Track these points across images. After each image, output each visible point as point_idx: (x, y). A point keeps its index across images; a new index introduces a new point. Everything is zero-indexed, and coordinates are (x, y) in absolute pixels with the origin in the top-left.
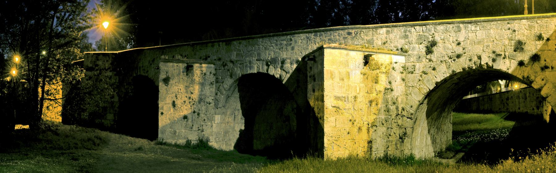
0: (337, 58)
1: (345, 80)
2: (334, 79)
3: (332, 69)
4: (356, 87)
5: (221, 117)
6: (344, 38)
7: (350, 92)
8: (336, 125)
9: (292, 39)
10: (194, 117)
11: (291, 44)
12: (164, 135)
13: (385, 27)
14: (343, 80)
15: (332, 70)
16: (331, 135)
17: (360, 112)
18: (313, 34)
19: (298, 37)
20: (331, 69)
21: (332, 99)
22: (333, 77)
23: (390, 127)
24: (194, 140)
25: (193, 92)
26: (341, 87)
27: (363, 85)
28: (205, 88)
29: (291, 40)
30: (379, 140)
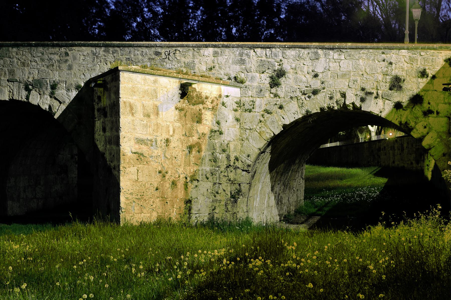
0: (140, 86)
1: (152, 117)
2: (135, 115)
3: (132, 101)
4: (168, 127)
6: (149, 59)
7: (159, 134)
8: (138, 179)
9: (69, 53)
11: (66, 61)
13: (212, 47)
14: (149, 116)
18: (103, 49)
20: (130, 100)
21: (132, 142)
23: (218, 181)
26: (146, 126)
29: (67, 54)
30: (201, 199)
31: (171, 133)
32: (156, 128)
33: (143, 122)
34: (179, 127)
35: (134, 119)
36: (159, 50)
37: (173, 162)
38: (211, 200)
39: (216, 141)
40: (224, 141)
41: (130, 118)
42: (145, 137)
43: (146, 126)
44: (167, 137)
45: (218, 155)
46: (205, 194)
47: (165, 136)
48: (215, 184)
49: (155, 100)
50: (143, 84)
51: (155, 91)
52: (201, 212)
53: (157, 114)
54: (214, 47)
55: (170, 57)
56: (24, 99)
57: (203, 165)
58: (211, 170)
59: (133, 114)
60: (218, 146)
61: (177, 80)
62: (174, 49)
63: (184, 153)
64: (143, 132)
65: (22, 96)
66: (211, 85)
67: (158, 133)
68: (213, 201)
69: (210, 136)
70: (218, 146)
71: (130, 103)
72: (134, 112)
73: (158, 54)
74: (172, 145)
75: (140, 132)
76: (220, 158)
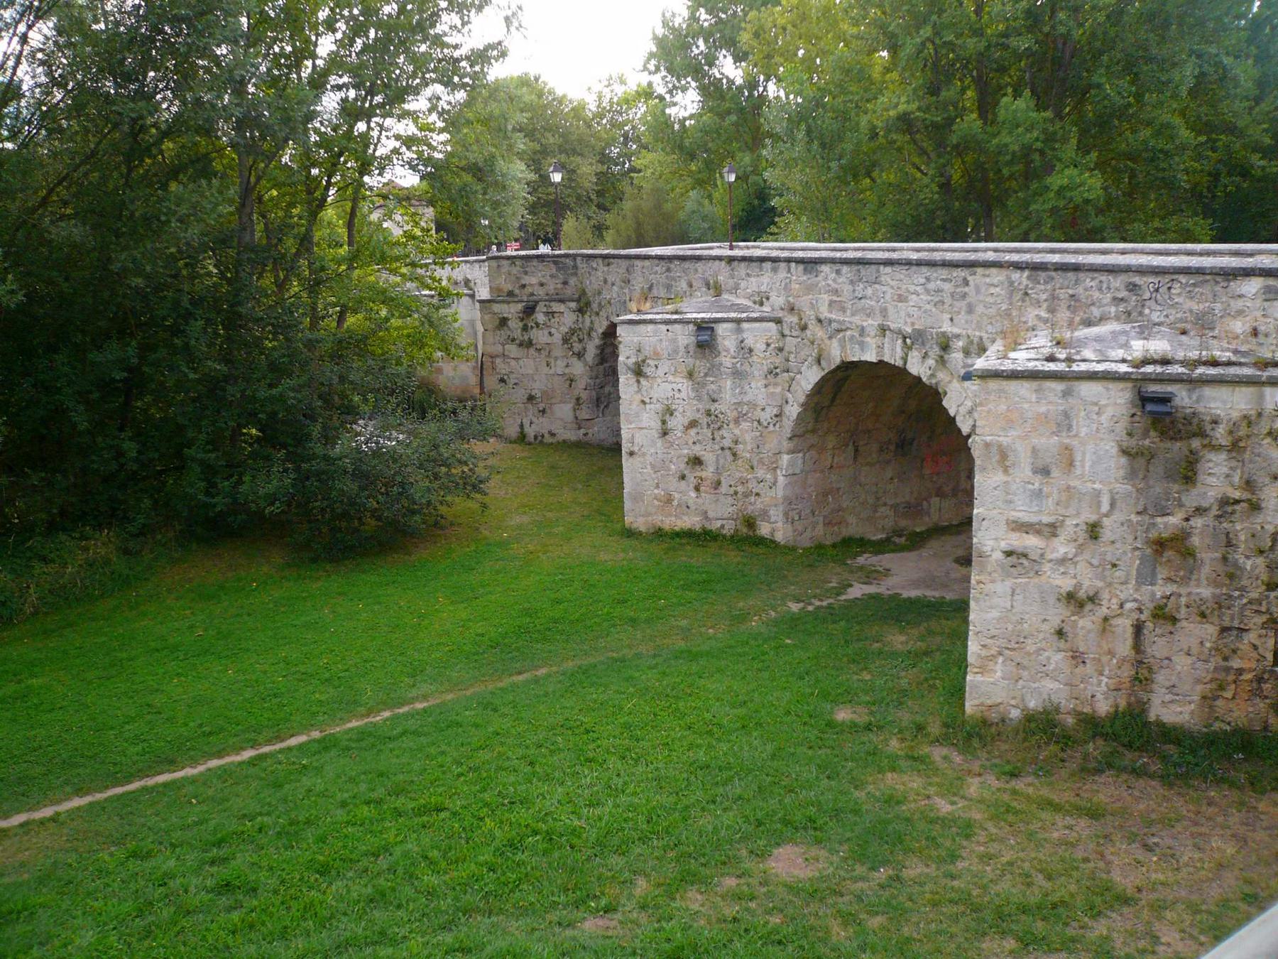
0: (1026, 406)
1: (1055, 473)
2: (1011, 471)
3: (1004, 441)
4: (1098, 494)
5: (804, 458)
6: (1115, 299)
7: (1071, 511)
8: (1012, 606)
9: (969, 278)
10: (722, 461)
11: (964, 296)
12: (637, 515)
13: (1260, 275)
14: (1045, 472)
15: (1005, 444)
16: (993, 632)
17: (1107, 573)
18: (1026, 273)
19: (984, 275)
20: (1001, 439)
21: (1001, 530)
22: (1007, 464)
23: (1236, 624)
24: (725, 516)
25: (715, 396)
26: (1038, 494)
27: (1130, 487)
28: (753, 385)
29: (966, 283)
30: (1182, 663)
31: (1105, 507)
32: (1063, 499)
33: (1030, 486)
34: (1129, 495)
35: (1009, 479)
36: (1137, 279)
37: (1107, 573)
38: (1211, 666)
39: (1238, 528)
40: (1262, 527)
41: (998, 477)
42: (1033, 519)
43: (1038, 494)
44: (1093, 518)
45: (1242, 560)
46: (1195, 651)
47: (1090, 516)
48: (1224, 630)
49: (1064, 434)
50: (1034, 400)
51: (1066, 415)
52: (1179, 692)
53: (1071, 464)
54: (1265, 276)
55: (1159, 296)
56: (899, 363)
57: (1193, 583)
58: (1214, 595)
59: (1006, 471)
60: (1243, 538)
61: (1130, 385)
62: (1168, 278)
63: (1137, 553)
64: (1030, 507)
65: (893, 354)
66: (1231, 389)
67: (1071, 509)
68: (1216, 668)
69: (1219, 513)
70: (1243, 538)
71: (1000, 446)
72: (1007, 464)
73: (1133, 288)
74: (1107, 534)
75: (1022, 508)
76: (1248, 568)
